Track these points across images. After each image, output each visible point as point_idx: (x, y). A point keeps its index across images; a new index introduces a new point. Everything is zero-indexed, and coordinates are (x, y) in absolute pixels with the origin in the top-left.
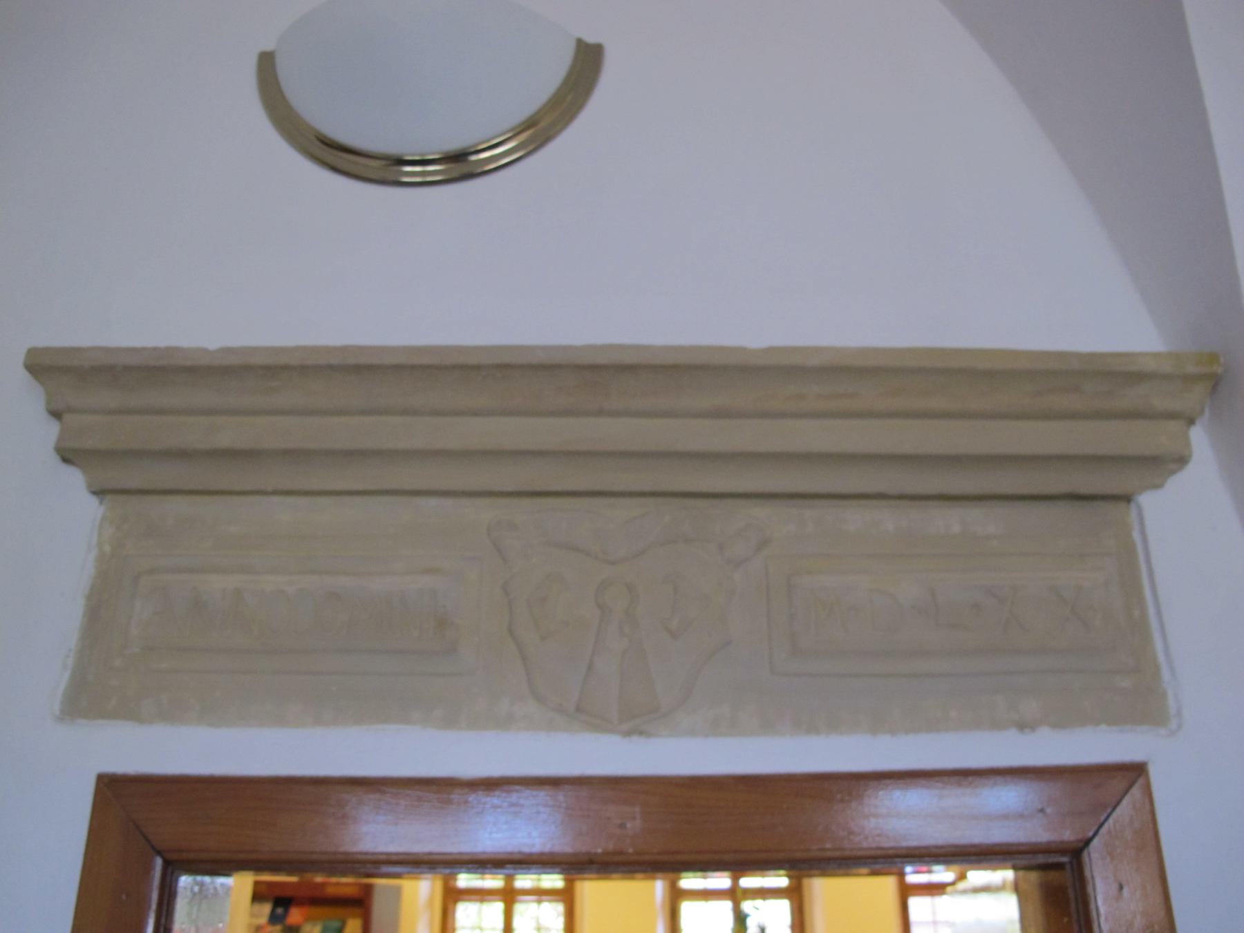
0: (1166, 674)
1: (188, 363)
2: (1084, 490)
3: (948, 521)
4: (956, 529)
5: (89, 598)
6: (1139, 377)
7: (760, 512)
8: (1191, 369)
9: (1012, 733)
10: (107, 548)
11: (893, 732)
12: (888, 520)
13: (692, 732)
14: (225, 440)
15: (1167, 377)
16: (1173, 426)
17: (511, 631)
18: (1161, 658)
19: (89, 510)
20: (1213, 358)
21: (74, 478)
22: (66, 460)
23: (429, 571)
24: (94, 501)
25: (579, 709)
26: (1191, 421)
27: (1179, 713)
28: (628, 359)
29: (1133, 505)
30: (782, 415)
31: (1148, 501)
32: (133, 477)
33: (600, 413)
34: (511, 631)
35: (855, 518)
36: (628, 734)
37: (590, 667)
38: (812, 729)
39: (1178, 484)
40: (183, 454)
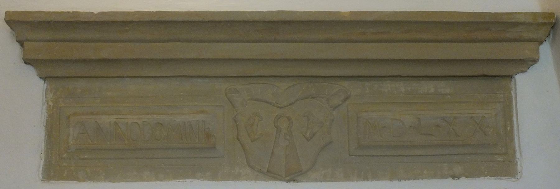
0: (518, 155)
1: (86, 20)
2: (490, 73)
3: (429, 87)
4: (432, 90)
5: (46, 127)
6: (517, 24)
7: (346, 84)
8: (541, 21)
9: (450, 180)
10: (51, 104)
11: (399, 180)
12: (402, 87)
13: (316, 180)
14: (104, 55)
15: (529, 24)
16: (532, 45)
17: (238, 139)
18: (517, 148)
19: (41, 85)
20: (551, 15)
21: (31, 73)
22: (25, 63)
23: (202, 112)
24: (42, 82)
25: (268, 171)
26: (541, 43)
27: (521, 172)
28: (288, 19)
29: (513, 80)
30: (357, 42)
31: (519, 78)
32: (59, 72)
33: (275, 41)
34: (238, 139)
35: (388, 86)
36: (288, 181)
37: (272, 153)
38: (366, 179)
39: (533, 71)
40: (85, 61)
